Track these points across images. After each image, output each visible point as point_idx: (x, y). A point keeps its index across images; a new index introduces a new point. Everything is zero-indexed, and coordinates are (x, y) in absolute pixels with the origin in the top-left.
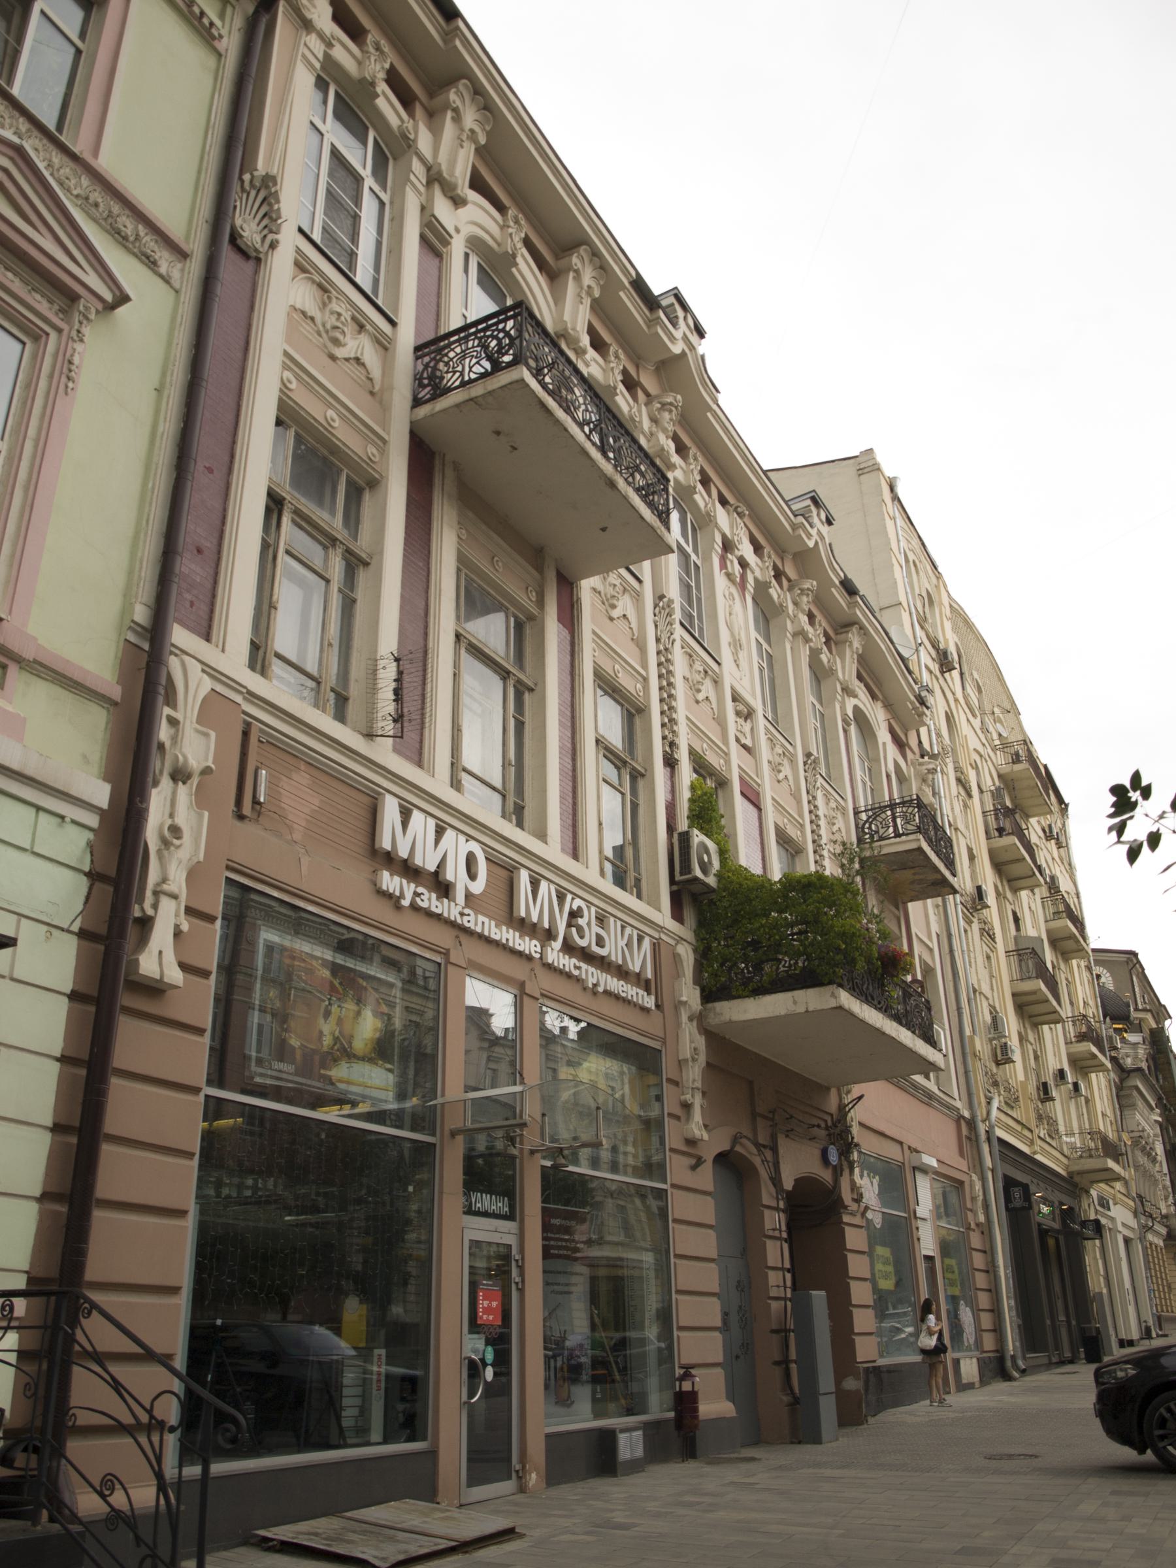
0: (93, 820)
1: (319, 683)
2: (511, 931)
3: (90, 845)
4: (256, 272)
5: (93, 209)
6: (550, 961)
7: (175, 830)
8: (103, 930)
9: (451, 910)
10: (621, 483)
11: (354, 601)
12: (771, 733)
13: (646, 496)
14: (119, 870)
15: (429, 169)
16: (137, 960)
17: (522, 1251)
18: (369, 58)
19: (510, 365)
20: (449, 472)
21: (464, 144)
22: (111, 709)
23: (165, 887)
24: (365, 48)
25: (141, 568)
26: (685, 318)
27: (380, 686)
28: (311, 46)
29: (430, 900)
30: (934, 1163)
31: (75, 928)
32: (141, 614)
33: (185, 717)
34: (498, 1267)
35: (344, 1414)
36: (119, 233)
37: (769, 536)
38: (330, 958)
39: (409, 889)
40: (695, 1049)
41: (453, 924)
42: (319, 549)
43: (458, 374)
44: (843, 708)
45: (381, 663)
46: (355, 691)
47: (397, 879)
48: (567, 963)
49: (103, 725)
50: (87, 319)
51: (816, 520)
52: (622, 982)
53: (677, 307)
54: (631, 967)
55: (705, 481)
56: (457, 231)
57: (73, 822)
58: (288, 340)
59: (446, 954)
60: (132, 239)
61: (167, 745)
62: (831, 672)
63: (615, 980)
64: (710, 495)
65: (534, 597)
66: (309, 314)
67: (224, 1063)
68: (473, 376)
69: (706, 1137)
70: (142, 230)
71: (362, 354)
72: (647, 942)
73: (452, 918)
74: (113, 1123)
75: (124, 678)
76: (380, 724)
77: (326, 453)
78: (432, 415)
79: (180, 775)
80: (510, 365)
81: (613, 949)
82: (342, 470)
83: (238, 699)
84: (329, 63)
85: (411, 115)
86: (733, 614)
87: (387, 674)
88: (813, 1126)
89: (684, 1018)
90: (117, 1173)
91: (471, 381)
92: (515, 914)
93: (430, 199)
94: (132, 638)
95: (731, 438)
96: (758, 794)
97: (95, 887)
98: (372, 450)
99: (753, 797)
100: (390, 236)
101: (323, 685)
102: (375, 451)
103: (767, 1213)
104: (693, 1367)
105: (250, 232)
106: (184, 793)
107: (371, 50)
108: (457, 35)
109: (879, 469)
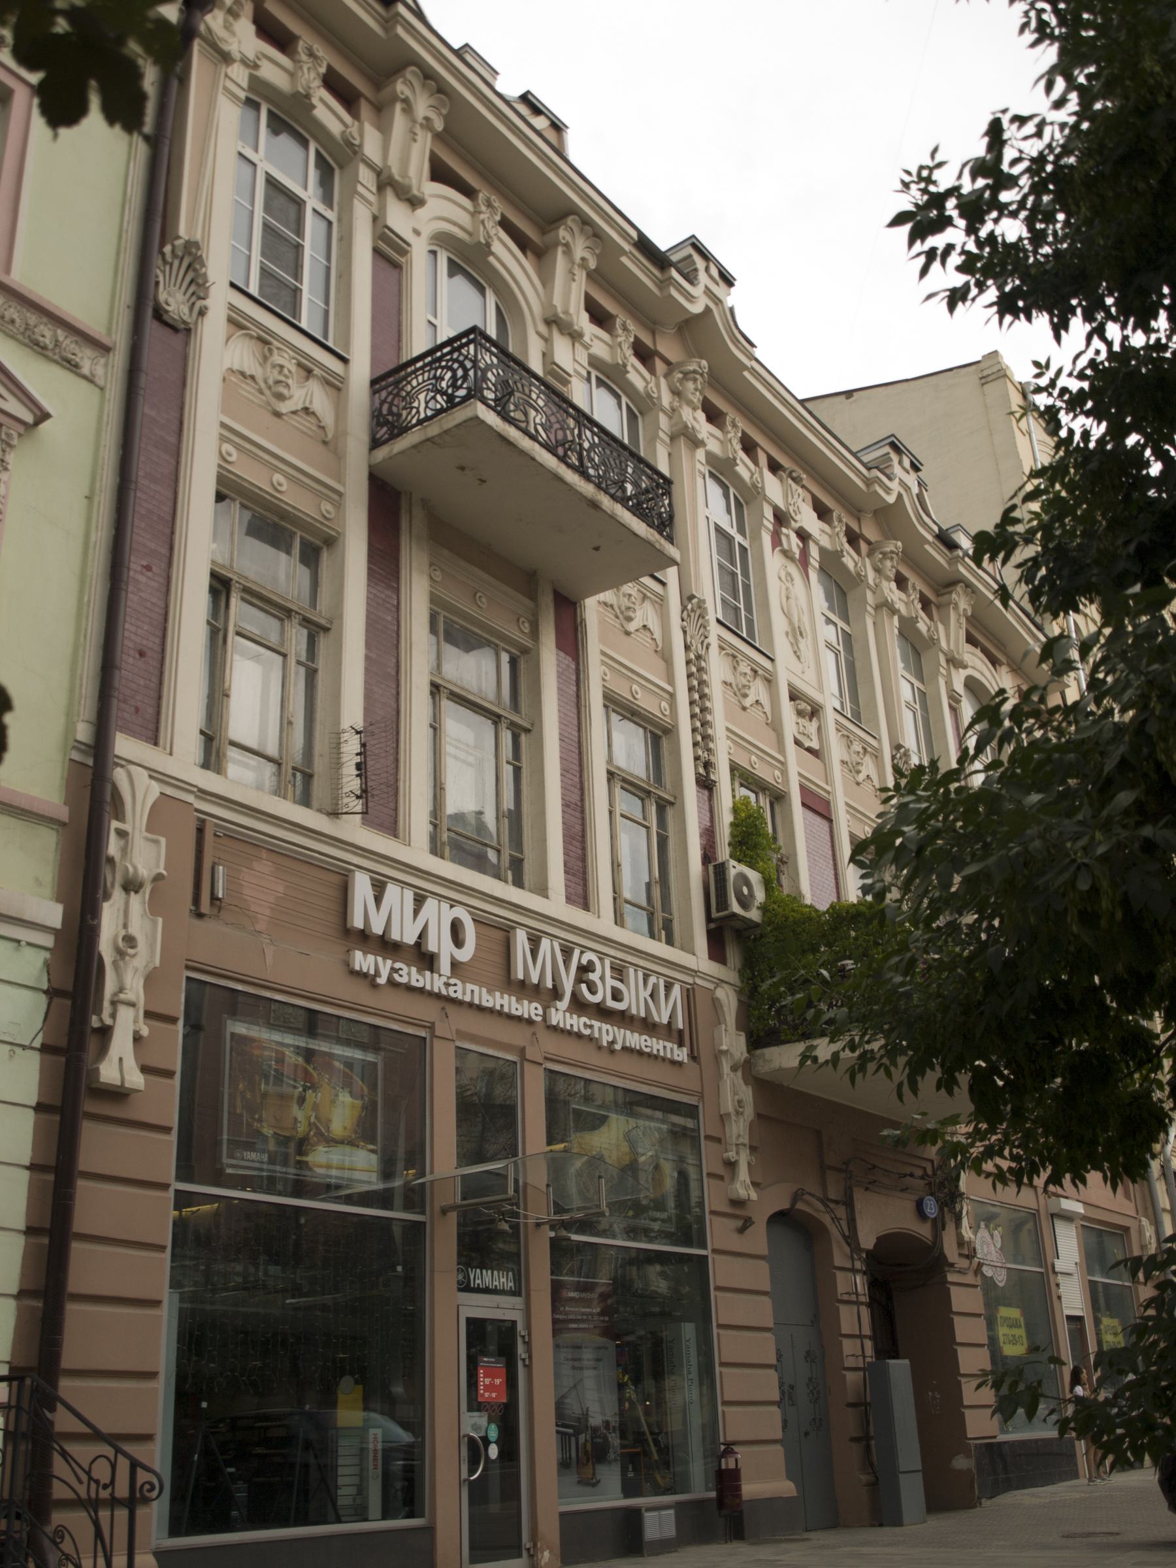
0: (48, 941)
1: (280, 764)
2: (506, 996)
3: (47, 965)
4: (187, 344)
5: (10, 327)
6: (554, 1023)
7: (130, 940)
8: (63, 1043)
9: (435, 982)
10: (606, 502)
11: (315, 671)
12: (847, 729)
13: (639, 504)
14: (75, 986)
15: (379, 174)
16: (98, 1069)
17: (528, 1326)
18: (301, 68)
19: (465, 399)
20: (418, 512)
21: (419, 138)
22: (60, 829)
23: (122, 996)
24: (297, 57)
25: (81, 685)
26: (707, 269)
27: (344, 760)
28: (233, 76)
29: (410, 975)
30: (1079, 1208)
31: (37, 1043)
32: (83, 732)
33: (134, 828)
34: (491, 1341)
35: (340, 1492)
36: (37, 344)
37: (834, 495)
38: (303, 1044)
39: (385, 966)
40: (739, 1102)
41: (438, 996)
42: (274, 624)
43: (414, 411)
44: (949, 683)
45: (345, 737)
46: (320, 766)
47: (371, 958)
48: (577, 1022)
49: (53, 846)
50: (10, 446)
51: (897, 469)
52: (645, 1037)
53: (697, 258)
54: (657, 1019)
55: (749, 447)
56: (417, 233)
57: (29, 944)
58: (225, 410)
59: (431, 1027)
60: (51, 346)
61: (117, 859)
62: (933, 642)
63: (636, 1035)
64: (756, 463)
65: (526, 628)
66: (248, 373)
67: (196, 1156)
68: (429, 413)
69: (754, 1196)
70: (61, 334)
71: (311, 402)
72: (676, 991)
73: (436, 990)
74: (82, 1222)
75: (71, 799)
76: (345, 800)
77: (276, 519)
78: (390, 458)
79: (131, 886)
80: (465, 399)
81: (634, 1000)
82: (295, 533)
83: (190, 798)
84: (257, 85)
85: (355, 115)
86: (793, 596)
87: (351, 747)
88: (905, 1175)
89: (726, 1068)
90: (88, 1268)
91: (427, 419)
92: (512, 977)
93: (382, 207)
94: (76, 756)
95: (777, 395)
96: (828, 803)
97: (53, 1004)
98: (326, 507)
99: (819, 806)
100: (340, 257)
101: (284, 766)
102: (329, 507)
103: (840, 1275)
104: (735, 1443)
105: (175, 302)
106: (137, 902)
107: (304, 57)
108: (397, 22)
109: (1005, 376)
